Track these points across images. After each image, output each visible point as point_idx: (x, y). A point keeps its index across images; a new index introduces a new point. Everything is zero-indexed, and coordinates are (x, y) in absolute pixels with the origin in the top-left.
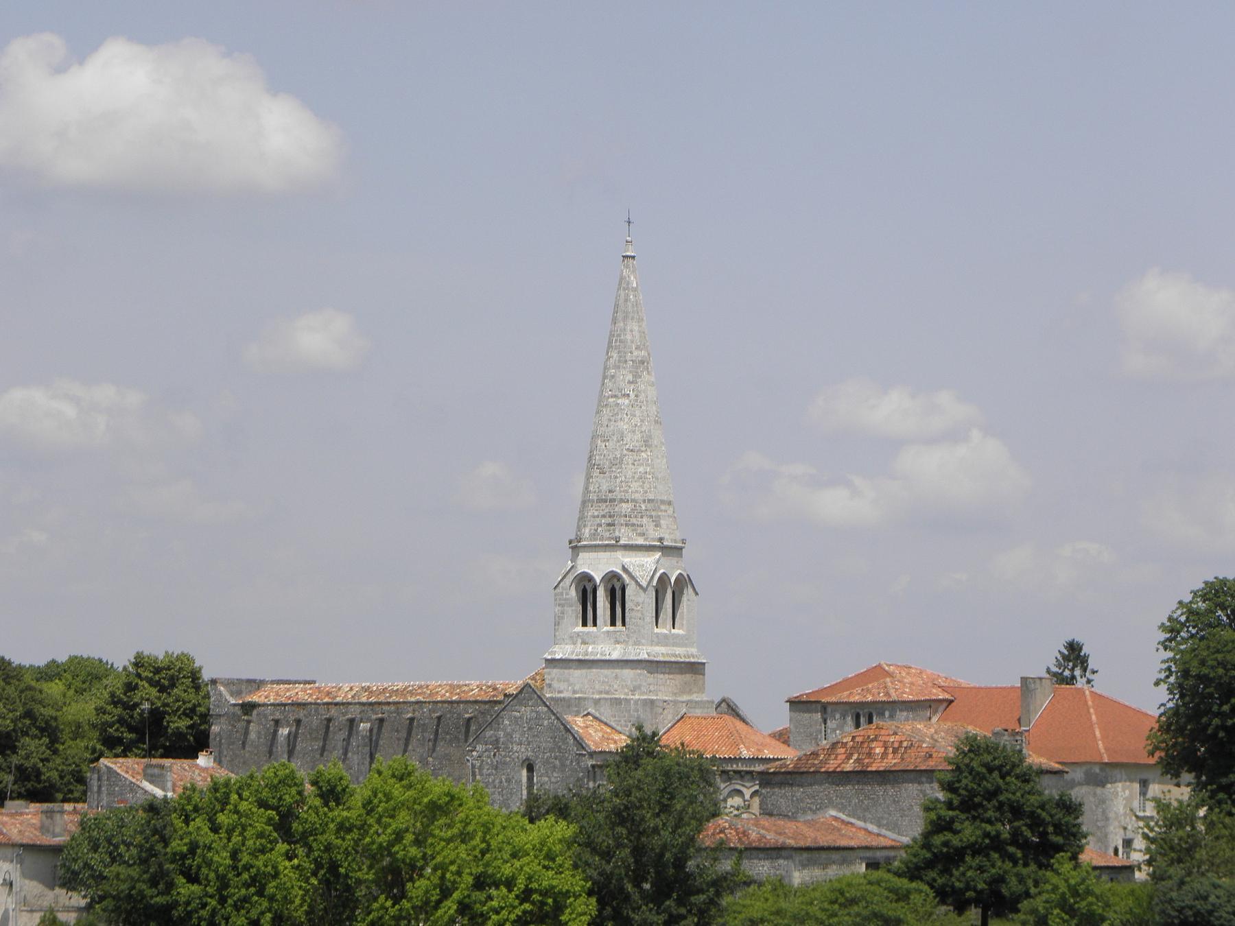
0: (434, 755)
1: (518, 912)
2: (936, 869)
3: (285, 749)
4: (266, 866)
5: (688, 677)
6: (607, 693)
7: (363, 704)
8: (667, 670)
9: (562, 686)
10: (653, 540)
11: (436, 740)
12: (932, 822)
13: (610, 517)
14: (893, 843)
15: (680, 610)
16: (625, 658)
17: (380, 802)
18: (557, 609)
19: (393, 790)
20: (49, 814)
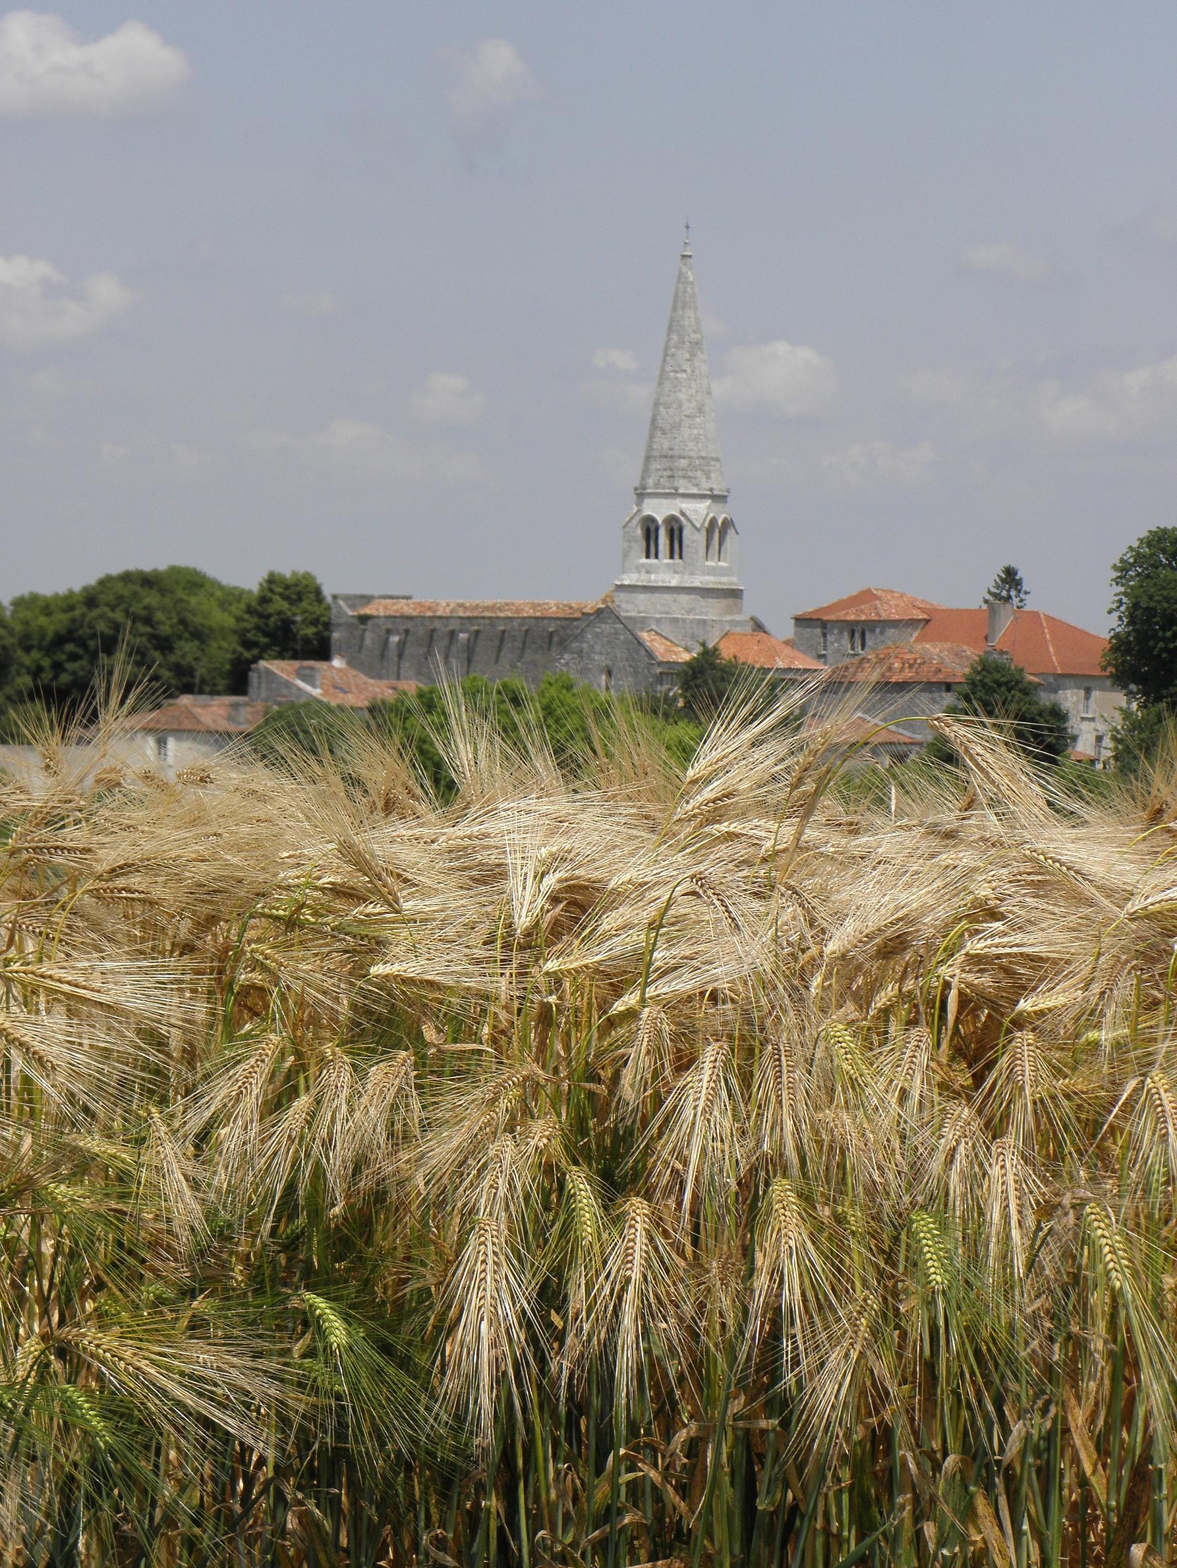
5: (730, 601)
6: (667, 613)
7: (461, 618)
9: (629, 607)
18: (626, 544)
20: (235, 706)
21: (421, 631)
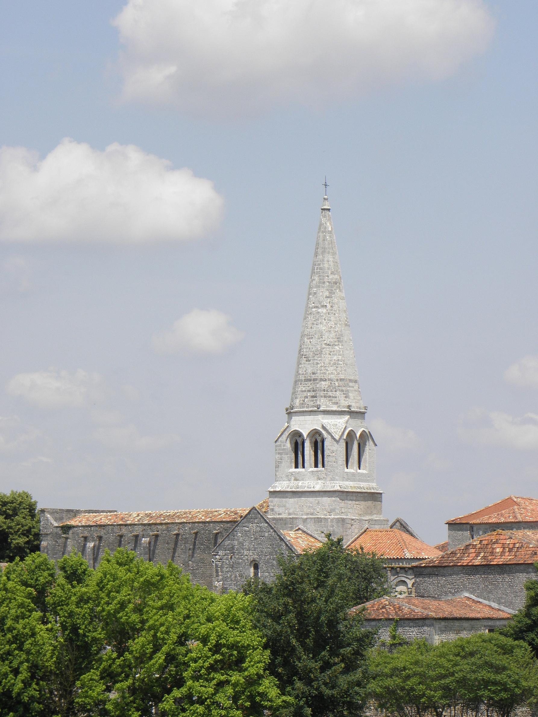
0: (193, 559)
1: (211, 661)
2: (534, 631)
3: (91, 557)
4: (24, 628)
5: (370, 503)
6: (312, 514)
7: (144, 525)
8: (355, 498)
10: (344, 407)
11: (194, 549)
12: (531, 598)
13: (314, 391)
14: (509, 616)
15: (364, 457)
16: (324, 490)
17: (109, 581)
18: (278, 456)
19: (118, 572)
21: (112, 538)
